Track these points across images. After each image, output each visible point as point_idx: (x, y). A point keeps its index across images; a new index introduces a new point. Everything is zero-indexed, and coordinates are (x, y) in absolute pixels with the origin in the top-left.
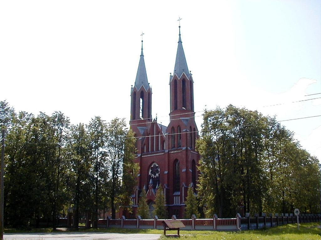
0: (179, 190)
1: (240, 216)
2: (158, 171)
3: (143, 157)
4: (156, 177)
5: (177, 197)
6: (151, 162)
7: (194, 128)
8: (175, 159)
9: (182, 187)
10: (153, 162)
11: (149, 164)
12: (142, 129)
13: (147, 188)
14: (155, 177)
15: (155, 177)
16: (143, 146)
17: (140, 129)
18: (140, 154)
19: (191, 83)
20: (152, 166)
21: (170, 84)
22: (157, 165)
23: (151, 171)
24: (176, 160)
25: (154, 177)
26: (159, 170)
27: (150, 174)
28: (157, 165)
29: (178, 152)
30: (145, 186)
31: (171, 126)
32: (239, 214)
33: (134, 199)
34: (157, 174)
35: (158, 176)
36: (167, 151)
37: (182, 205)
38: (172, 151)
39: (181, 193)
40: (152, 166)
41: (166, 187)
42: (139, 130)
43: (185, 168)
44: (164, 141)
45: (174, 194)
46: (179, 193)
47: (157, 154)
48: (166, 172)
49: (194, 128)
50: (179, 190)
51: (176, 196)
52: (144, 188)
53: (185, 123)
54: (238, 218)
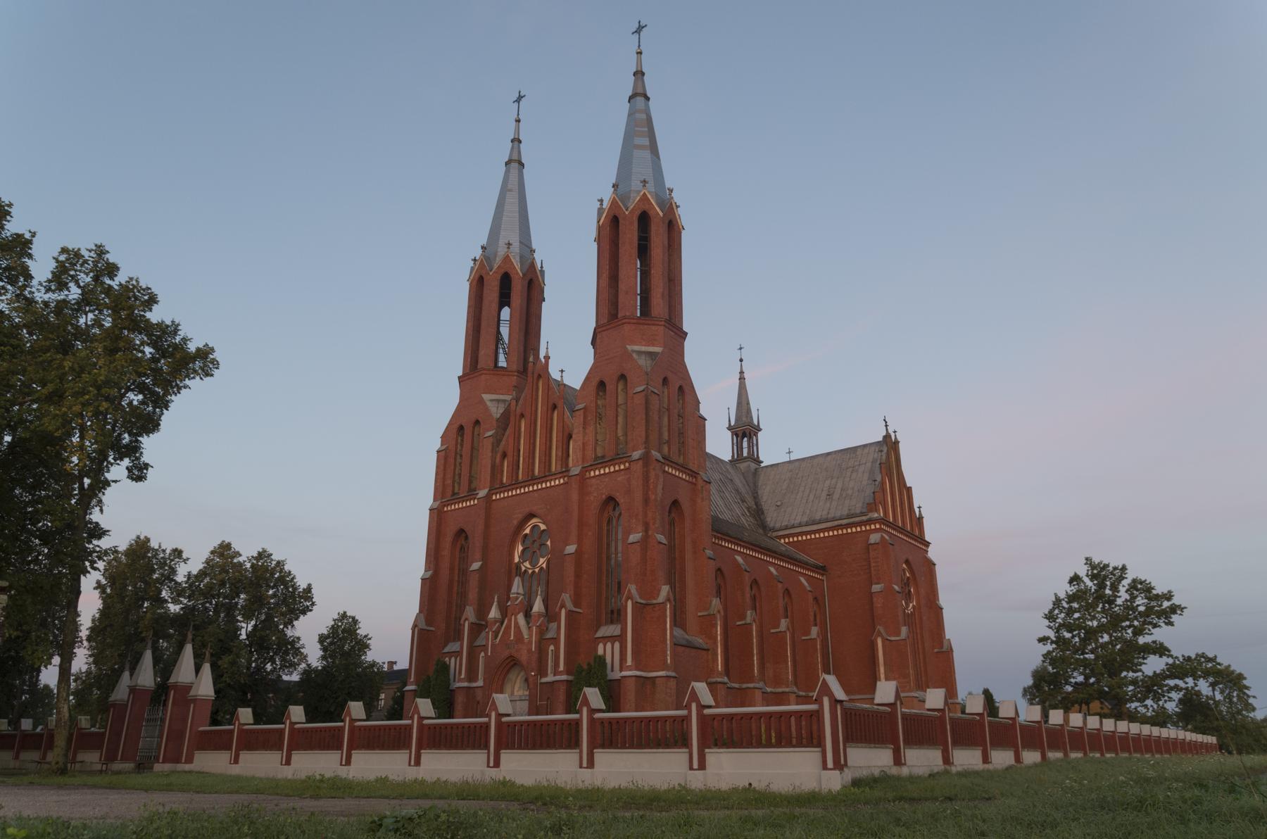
0: (616, 616)
1: (840, 694)
2: (547, 545)
3: (448, 511)
4: (537, 570)
5: (609, 645)
6: (520, 516)
7: (681, 388)
8: (604, 496)
9: (626, 602)
10: (532, 516)
11: (515, 522)
12: (498, 401)
13: (504, 611)
14: (534, 572)
15: (534, 572)
16: (498, 460)
17: (492, 400)
18: (484, 488)
19: (673, 228)
20: (527, 531)
21: (599, 240)
22: (543, 527)
23: (521, 548)
24: (611, 501)
25: (530, 571)
26: (549, 543)
27: (517, 560)
28: (543, 527)
29: (615, 471)
30: (495, 603)
31: (456, 426)
32: (832, 681)
33: (458, 659)
34: (542, 560)
35: (544, 566)
36: (575, 471)
37: (625, 673)
38: (594, 466)
39: (624, 630)
40: (527, 531)
41: (570, 606)
42: (489, 404)
43: (640, 528)
44: (570, 437)
45: (599, 634)
46: (613, 630)
47: (506, 495)
48: (571, 549)
49: (681, 388)
50: (616, 616)
51: (605, 639)
52: (494, 613)
53: (643, 362)
54: (826, 701)
